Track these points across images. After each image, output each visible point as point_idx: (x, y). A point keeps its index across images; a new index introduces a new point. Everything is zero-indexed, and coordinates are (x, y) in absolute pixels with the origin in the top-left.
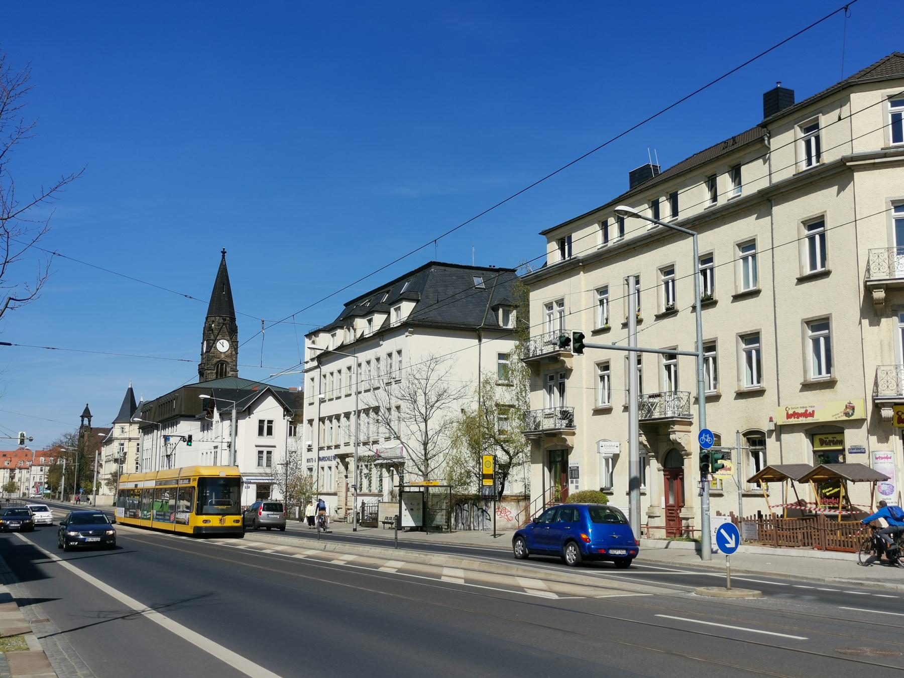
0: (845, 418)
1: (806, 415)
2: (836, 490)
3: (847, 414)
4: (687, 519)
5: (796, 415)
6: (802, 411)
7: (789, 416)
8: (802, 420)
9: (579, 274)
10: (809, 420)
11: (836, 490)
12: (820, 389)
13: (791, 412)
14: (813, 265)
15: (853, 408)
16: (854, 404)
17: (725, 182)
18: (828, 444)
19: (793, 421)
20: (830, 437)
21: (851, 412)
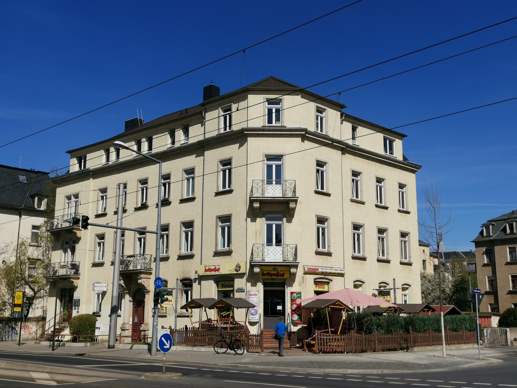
0: (235, 272)
1: (215, 270)
2: (228, 313)
3: (236, 270)
4: (145, 331)
5: (210, 270)
6: (213, 268)
8: (213, 273)
9: (89, 179)
10: (217, 273)
11: (228, 313)
12: (223, 256)
13: (207, 268)
14: (224, 187)
15: (240, 267)
16: (241, 264)
17: (180, 135)
18: (226, 287)
19: (208, 273)
20: (227, 283)
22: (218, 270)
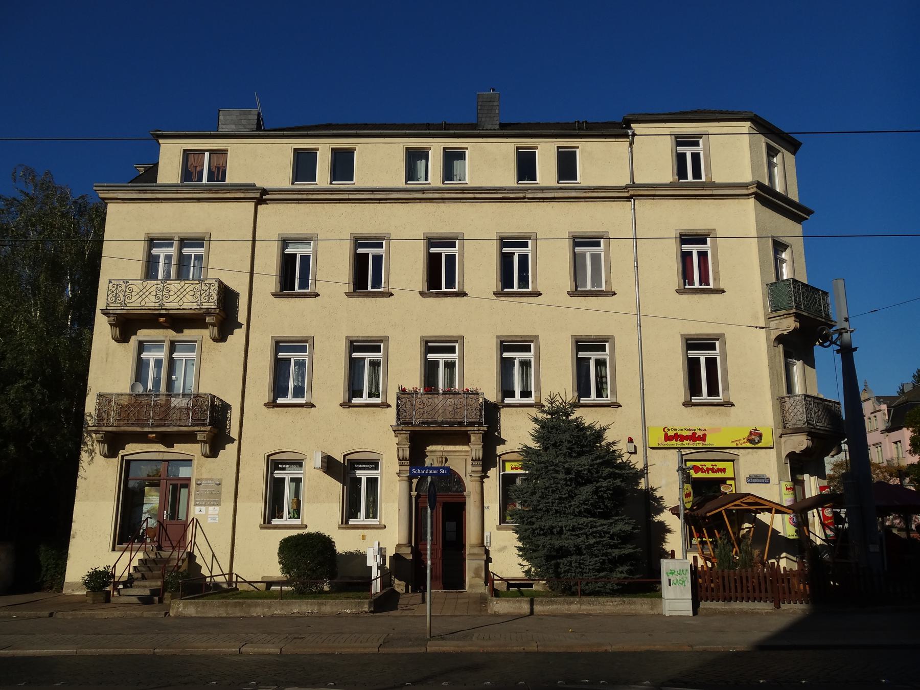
1: (693, 437)
5: (677, 437)
7: (667, 438)
13: (671, 433)
15: (760, 436)
21: (757, 439)
22: (703, 438)
